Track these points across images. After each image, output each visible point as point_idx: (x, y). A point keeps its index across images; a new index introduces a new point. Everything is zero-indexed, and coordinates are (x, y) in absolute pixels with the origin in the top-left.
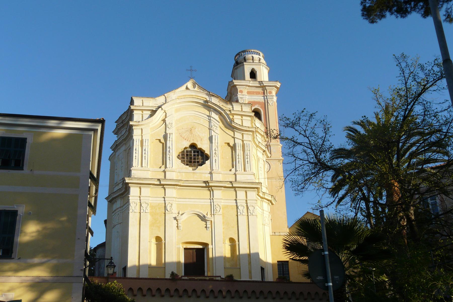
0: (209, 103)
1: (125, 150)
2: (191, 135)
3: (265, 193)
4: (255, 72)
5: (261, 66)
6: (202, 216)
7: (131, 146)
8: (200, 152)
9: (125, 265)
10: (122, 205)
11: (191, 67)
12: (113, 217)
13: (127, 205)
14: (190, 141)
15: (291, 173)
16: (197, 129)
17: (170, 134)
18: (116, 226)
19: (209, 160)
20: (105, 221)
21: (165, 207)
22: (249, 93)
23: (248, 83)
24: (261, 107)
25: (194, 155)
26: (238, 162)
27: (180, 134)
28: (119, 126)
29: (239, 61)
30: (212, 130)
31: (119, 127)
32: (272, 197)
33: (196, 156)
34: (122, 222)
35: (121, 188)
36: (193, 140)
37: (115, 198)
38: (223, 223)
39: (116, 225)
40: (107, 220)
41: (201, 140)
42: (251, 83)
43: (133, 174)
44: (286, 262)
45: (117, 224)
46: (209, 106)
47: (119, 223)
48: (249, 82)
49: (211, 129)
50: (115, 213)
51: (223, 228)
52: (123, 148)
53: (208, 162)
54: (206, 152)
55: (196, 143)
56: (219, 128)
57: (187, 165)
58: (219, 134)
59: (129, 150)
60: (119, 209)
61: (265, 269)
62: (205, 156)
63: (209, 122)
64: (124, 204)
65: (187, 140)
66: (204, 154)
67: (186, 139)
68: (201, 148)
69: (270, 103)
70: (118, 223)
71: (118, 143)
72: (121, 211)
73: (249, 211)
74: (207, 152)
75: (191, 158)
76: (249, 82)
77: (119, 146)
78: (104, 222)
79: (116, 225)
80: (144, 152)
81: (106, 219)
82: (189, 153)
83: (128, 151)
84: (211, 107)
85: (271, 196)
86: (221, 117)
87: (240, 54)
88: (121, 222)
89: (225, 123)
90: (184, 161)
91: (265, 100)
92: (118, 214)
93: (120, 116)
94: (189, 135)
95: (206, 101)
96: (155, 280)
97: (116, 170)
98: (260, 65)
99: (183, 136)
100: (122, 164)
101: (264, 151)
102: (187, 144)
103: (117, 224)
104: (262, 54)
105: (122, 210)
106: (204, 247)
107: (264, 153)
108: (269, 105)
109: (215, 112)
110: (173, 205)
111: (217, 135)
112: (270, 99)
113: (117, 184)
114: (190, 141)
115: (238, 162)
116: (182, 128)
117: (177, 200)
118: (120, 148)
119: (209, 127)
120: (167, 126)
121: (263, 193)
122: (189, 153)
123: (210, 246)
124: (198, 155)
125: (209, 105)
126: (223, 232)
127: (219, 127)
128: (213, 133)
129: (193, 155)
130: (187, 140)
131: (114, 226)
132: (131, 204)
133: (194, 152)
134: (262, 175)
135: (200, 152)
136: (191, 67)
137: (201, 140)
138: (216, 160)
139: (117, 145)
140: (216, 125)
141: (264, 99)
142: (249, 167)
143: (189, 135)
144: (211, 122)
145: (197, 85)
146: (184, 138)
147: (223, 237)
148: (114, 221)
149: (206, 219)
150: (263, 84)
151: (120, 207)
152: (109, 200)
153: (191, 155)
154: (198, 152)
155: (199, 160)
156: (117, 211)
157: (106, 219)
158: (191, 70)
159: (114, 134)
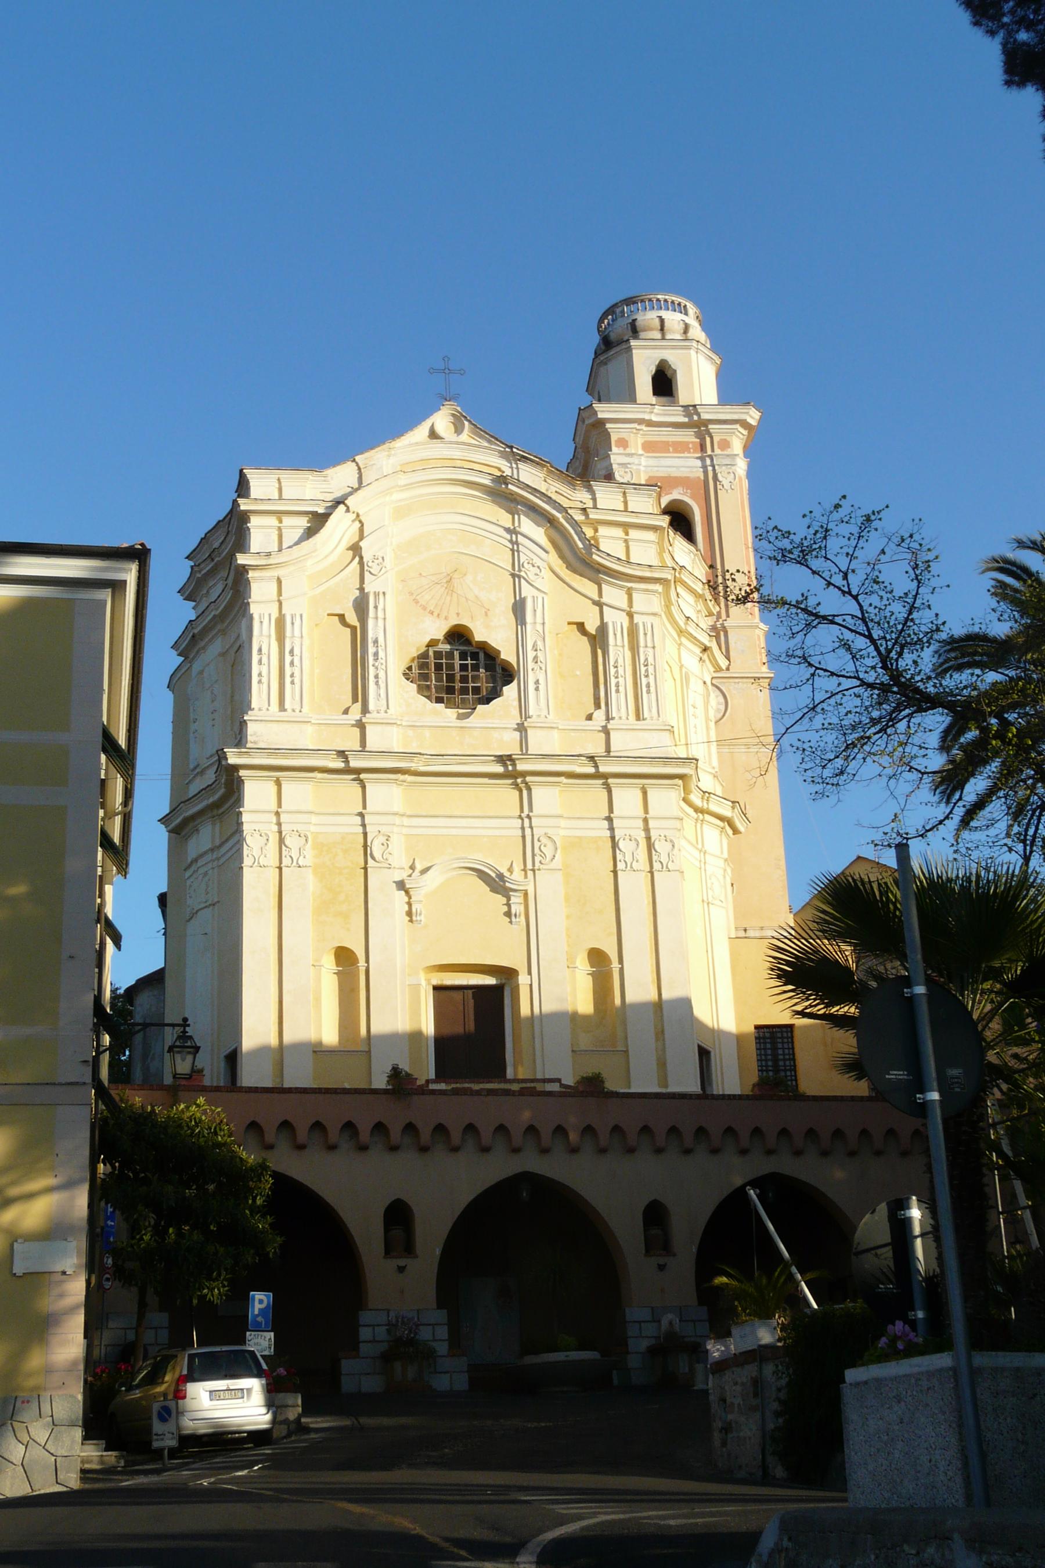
0: (510, 486)
1: (223, 654)
2: (448, 598)
3: (709, 793)
4: (669, 374)
5: (693, 352)
8: (482, 656)
10: (217, 842)
11: (446, 359)
14: (446, 618)
17: (376, 595)
18: (200, 912)
20: (163, 899)
22: (650, 447)
23: (644, 412)
24: (692, 497)
25: (463, 668)
26: (614, 688)
27: (411, 594)
29: (613, 337)
30: (522, 580)
31: (199, 575)
32: (733, 808)
34: (218, 902)
36: (458, 614)
39: (197, 912)
40: (168, 896)
41: (486, 614)
42: (655, 411)
44: (784, 1030)
48: (648, 410)
49: (519, 577)
50: (193, 868)
51: (568, 917)
53: (510, 691)
54: (503, 656)
56: (546, 573)
57: (439, 700)
60: (209, 857)
61: (712, 1054)
62: (499, 670)
63: (512, 550)
65: (435, 614)
66: (498, 662)
67: (432, 613)
68: (486, 642)
69: (725, 482)
70: (206, 902)
71: (199, 628)
72: (215, 863)
73: (655, 858)
74: (508, 655)
75: (451, 678)
76: (648, 410)
79: (197, 912)
80: (288, 659)
81: (164, 889)
82: (444, 661)
84: (518, 498)
85: (730, 804)
86: (552, 532)
87: (618, 310)
88: (216, 900)
90: (428, 687)
91: (706, 472)
92: (206, 874)
98: (688, 348)
100: (213, 701)
101: (705, 649)
104: (695, 309)
105: (218, 859)
106: (504, 981)
107: (705, 657)
108: (719, 487)
109: (531, 514)
111: (540, 595)
112: (724, 468)
113: (198, 770)
114: (446, 618)
115: (614, 688)
117: (406, 821)
119: (514, 570)
120: (366, 568)
121: (704, 792)
123: (523, 979)
124: (476, 668)
125: (512, 493)
128: (527, 591)
129: (457, 667)
130: (435, 614)
133: (463, 656)
135: (482, 656)
137: (486, 614)
138: (537, 682)
139: (193, 636)
141: (704, 467)
144: (518, 551)
145: (466, 423)
146: (424, 608)
147: (569, 945)
148: (190, 897)
150: (699, 415)
151: (212, 850)
153: (450, 667)
154: (475, 656)
158: (447, 371)
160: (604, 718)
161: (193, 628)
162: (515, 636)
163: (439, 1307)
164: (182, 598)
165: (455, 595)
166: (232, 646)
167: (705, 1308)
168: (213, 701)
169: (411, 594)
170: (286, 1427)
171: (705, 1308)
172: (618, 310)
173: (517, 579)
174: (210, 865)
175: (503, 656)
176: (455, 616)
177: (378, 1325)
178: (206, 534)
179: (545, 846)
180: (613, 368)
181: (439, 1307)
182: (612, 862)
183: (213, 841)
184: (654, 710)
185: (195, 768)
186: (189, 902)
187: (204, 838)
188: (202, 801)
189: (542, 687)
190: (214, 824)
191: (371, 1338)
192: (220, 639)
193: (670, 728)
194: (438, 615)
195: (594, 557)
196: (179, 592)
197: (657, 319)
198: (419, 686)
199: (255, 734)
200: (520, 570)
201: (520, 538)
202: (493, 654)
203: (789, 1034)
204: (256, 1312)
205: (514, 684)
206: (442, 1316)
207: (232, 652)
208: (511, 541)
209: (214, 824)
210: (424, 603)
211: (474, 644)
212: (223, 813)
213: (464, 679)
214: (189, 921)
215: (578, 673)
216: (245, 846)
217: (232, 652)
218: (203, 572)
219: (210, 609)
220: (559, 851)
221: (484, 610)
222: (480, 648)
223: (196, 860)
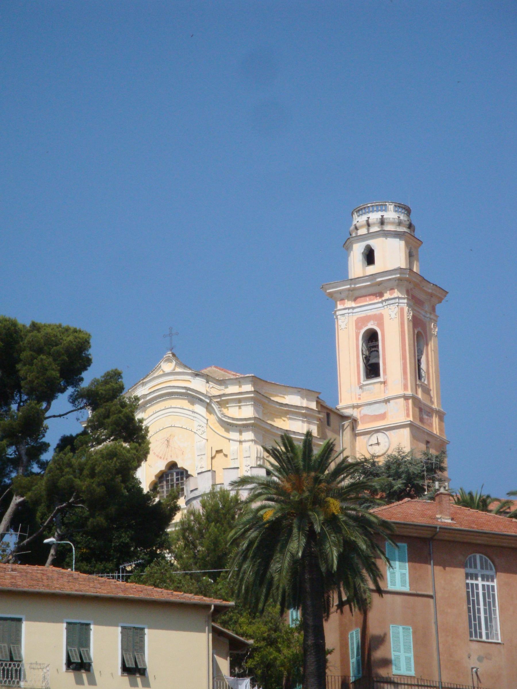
25: (177, 480)
41: (183, 454)
116: (156, 440)
130: (162, 458)
201: (195, 415)
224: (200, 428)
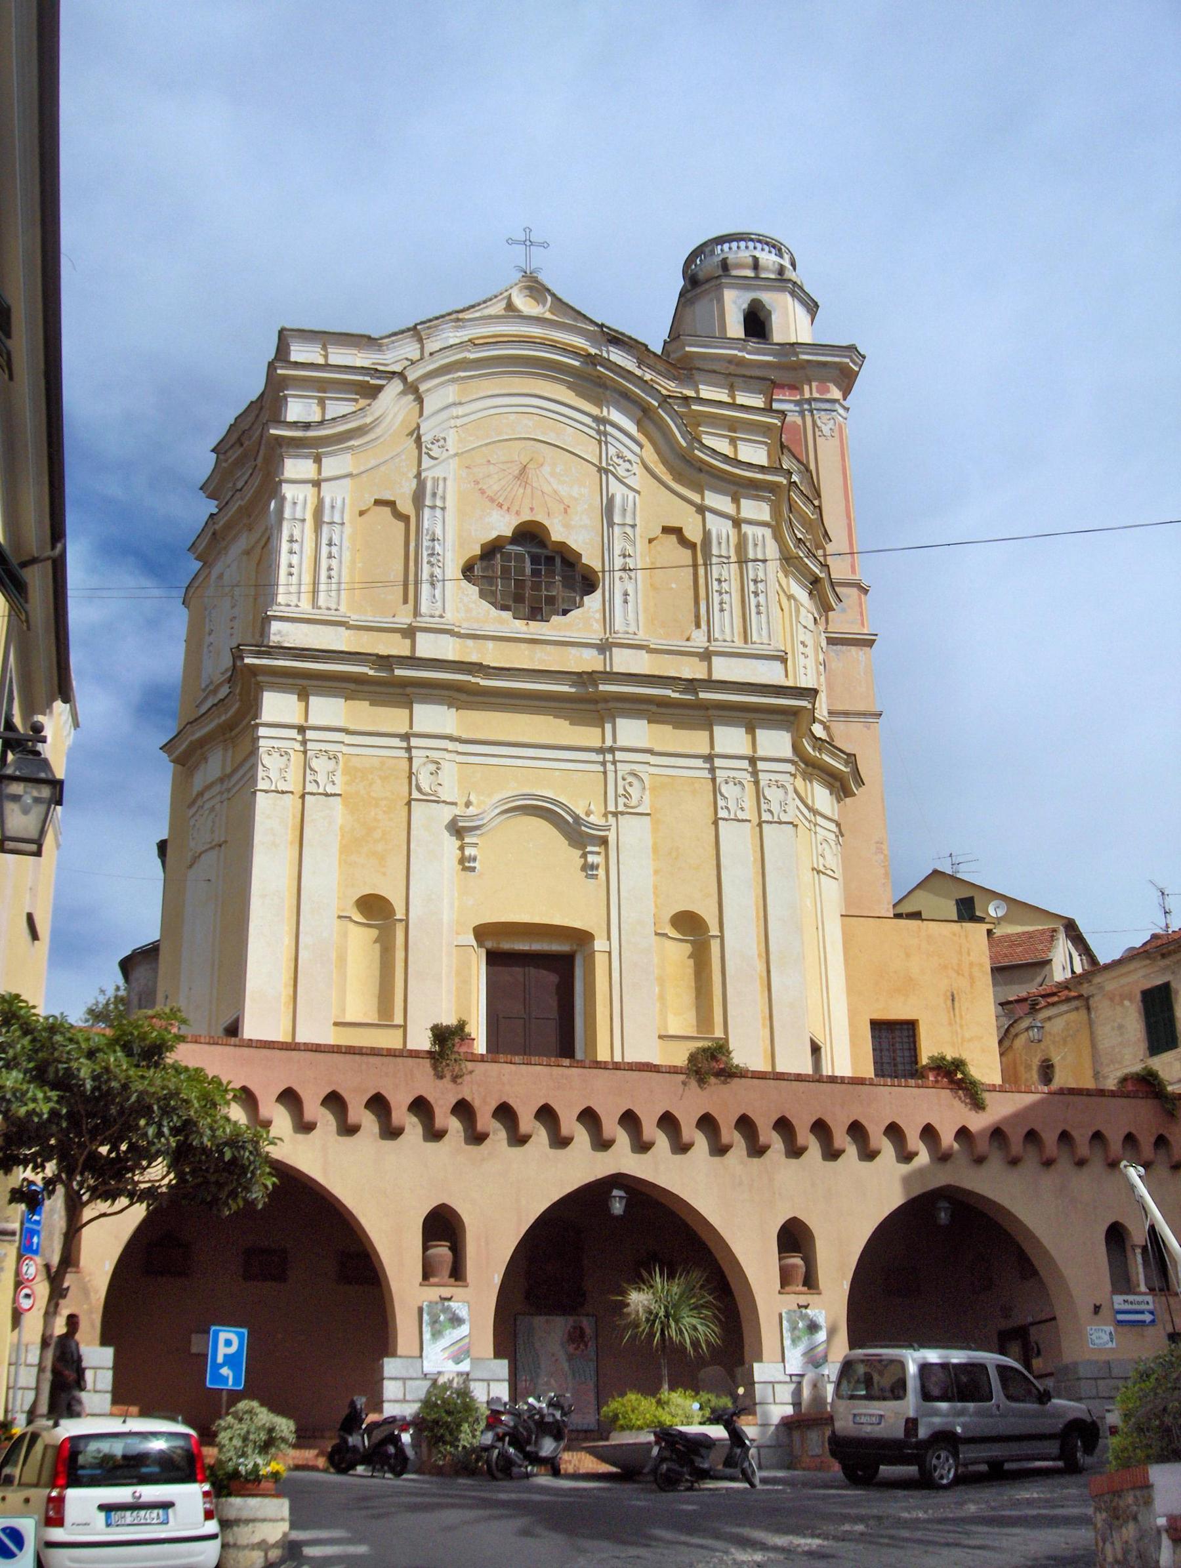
1: (248, 553)
4: (762, 315)
6: (570, 820)
7: (273, 522)
8: (558, 561)
9: (235, 1016)
10: (228, 770)
11: (528, 230)
12: (192, 822)
13: (247, 766)
14: (518, 513)
15: (410, 1357)
16: (546, 469)
17: (436, 481)
18: (203, 856)
19: (599, 592)
20: (162, 847)
21: (411, 773)
25: (535, 573)
26: (717, 607)
27: (476, 482)
28: (226, 461)
29: (701, 275)
30: (610, 475)
31: (224, 465)
33: (541, 582)
34: (226, 842)
35: (226, 697)
36: (532, 509)
37: (202, 743)
38: (655, 850)
39: (200, 854)
40: (169, 844)
41: (566, 512)
43: (275, 634)
44: (905, 1027)
45: (206, 851)
46: (599, 377)
47: (214, 843)
49: (607, 471)
50: (199, 803)
51: (656, 872)
52: (243, 542)
53: (592, 602)
54: (584, 560)
55: (546, 523)
56: (637, 469)
57: (505, 608)
58: (638, 492)
59: (263, 548)
60: (217, 789)
61: (823, 1050)
62: (578, 578)
63: (600, 442)
64: (235, 765)
65: (505, 507)
66: (578, 568)
67: (500, 506)
69: (826, 430)
70: (210, 843)
71: (221, 523)
72: (225, 796)
73: (764, 807)
74: (590, 559)
75: (520, 584)
77: (224, 539)
78: (156, 847)
79: (200, 854)
80: (325, 550)
81: (165, 837)
82: (513, 563)
83: (259, 551)
87: (707, 250)
88: (223, 839)
89: (664, 448)
90: (494, 593)
92: (212, 809)
93: (232, 422)
94: (515, 489)
95: (591, 360)
96: (362, 1054)
97: (210, 634)
99: (489, 493)
100: (233, 607)
102: (503, 525)
103: (206, 851)
105: (229, 790)
106: (575, 947)
108: (818, 433)
109: (623, 402)
110: (445, 765)
111: (631, 494)
112: (823, 413)
113: (211, 687)
114: (518, 513)
115: (717, 607)
116: (489, 461)
118: (225, 548)
119: (601, 462)
120: (424, 450)
122: (513, 563)
123: (599, 944)
124: (551, 573)
125: (600, 376)
126: (656, 888)
127: (639, 462)
128: (615, 488)
129: (528, 571)
130: (505, 507)
131: (196, 859)
132: (265, 759)
133: (535, 560)
134: (809, 672)
135: (558, 561)
136: (528, 230)
137: (566, 512)
138: (626, 594)
139: (214, 534)
140: (630, 456)
142: (764, 626)
143: (515, 489)
144: (606, 443)
145: (549, 298)
146: (492, 500)
147: (656, 906)
148: (193, 839)
149: (583, 828)
151: (221, 780)
152: (177, 753)
153: (521, 571)
155: (554, 593)
156: (207, 796)
157: (166, 837)
158: (528, 243)
159: (207, 497)
160: (706, 638)
161: (214, 523)
162: (600, 539)
163: (498, 1354)
164: (204, 495)
165: (529, 490)
166: (257, 542)
167: (505, 1362)
168: (233, 607)
169: (476, 482)
170: (262, 1554)
171: (505, 1362)
172: (707, 250)
173: (604, 477)
174: (218, 798)
175: (584, 560)
176: (528, 511)
177: (411, 1379)
178: (236, 419)
179: (631, 786)
180: (701, 308)
181: (498, 1354)
182: (712, 809)
183: (223, 768)
184: (764, 632)
185: (207, 686)
186: (192, 844)
187: (214, 765)
188: (212, 721)
189: (630, 599)
190: (226, 750)
191: (401, 1396)
192: (245, 536)
193: (783, 654)
194: (509, 509)
195: (696, 452)
196: (201, 489)
197: (751, 259)
198: (481, 591)
199: (279, 632)
200: (608, 464)
201: (609, 429)
202: (571, 560)
203: (911, 1033)
204: (220, 1359)
205: (597, 594)
206: (502, 1367)
207: (258, 550)
208: (599, 432)
209: (226, 750)
210: (491, 494)
211: (550, 547)
212: (236, 736)
213: (536, 587)
214: (191, 866)
215: (674, 586)
216: (260, 767)
217: (258, 550)
218: (230, 461)
219: (235, 498)
220: (647, 792)
221: (562, 507)
222: (557, 552)
223: (201, 794)
224: (620, 461)
